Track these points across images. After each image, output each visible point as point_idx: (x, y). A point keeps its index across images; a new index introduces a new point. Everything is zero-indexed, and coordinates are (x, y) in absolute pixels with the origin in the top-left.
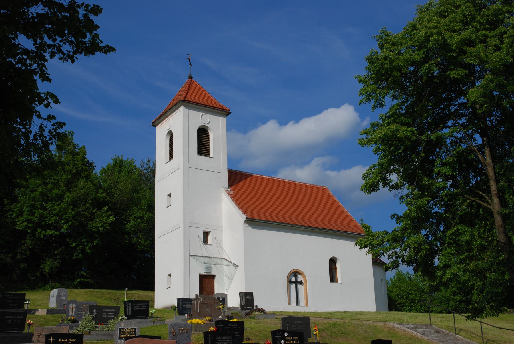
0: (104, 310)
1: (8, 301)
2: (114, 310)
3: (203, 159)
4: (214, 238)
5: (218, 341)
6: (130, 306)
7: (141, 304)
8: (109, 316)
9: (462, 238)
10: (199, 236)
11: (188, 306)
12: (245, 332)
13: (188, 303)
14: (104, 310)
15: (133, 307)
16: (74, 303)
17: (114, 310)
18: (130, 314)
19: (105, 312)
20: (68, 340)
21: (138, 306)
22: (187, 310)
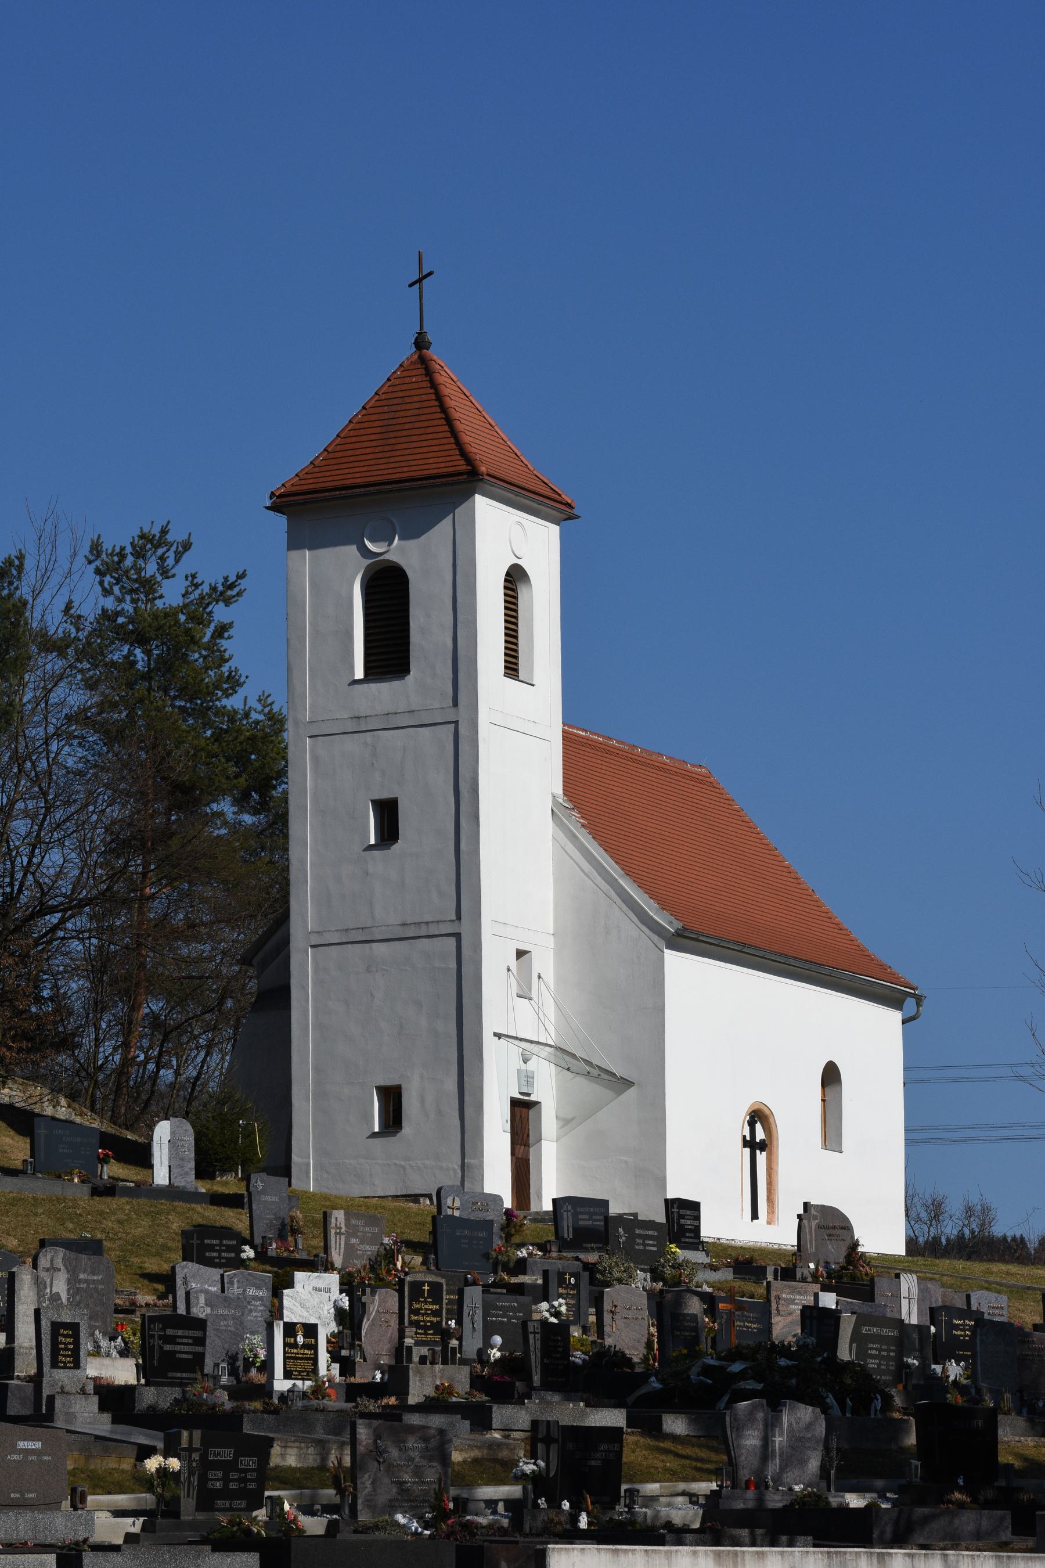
0: (637, 1231)
1: (61, 1151)
2: (656, 1233)
3: (385, 795)
4: (523, 947)
5: (191, 1341)
6: (569, 1213)
7: (592, 1210)
8: (648, 1248)
9: (369, 1476)
10: (509, 970)
11: (689, 1222)
12: (595, 1422)
13: (688, 1212)
14: (637, 1231)
15: (575, 1216)
16: (457, 1196)
17: (656, 1233)
18: (571, 1236)
19: (640, 1236)
20: (221, 1242)
21: (585, 1213)
22: (687, 1234)
